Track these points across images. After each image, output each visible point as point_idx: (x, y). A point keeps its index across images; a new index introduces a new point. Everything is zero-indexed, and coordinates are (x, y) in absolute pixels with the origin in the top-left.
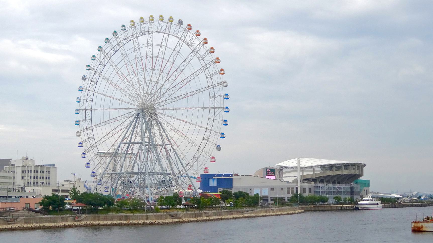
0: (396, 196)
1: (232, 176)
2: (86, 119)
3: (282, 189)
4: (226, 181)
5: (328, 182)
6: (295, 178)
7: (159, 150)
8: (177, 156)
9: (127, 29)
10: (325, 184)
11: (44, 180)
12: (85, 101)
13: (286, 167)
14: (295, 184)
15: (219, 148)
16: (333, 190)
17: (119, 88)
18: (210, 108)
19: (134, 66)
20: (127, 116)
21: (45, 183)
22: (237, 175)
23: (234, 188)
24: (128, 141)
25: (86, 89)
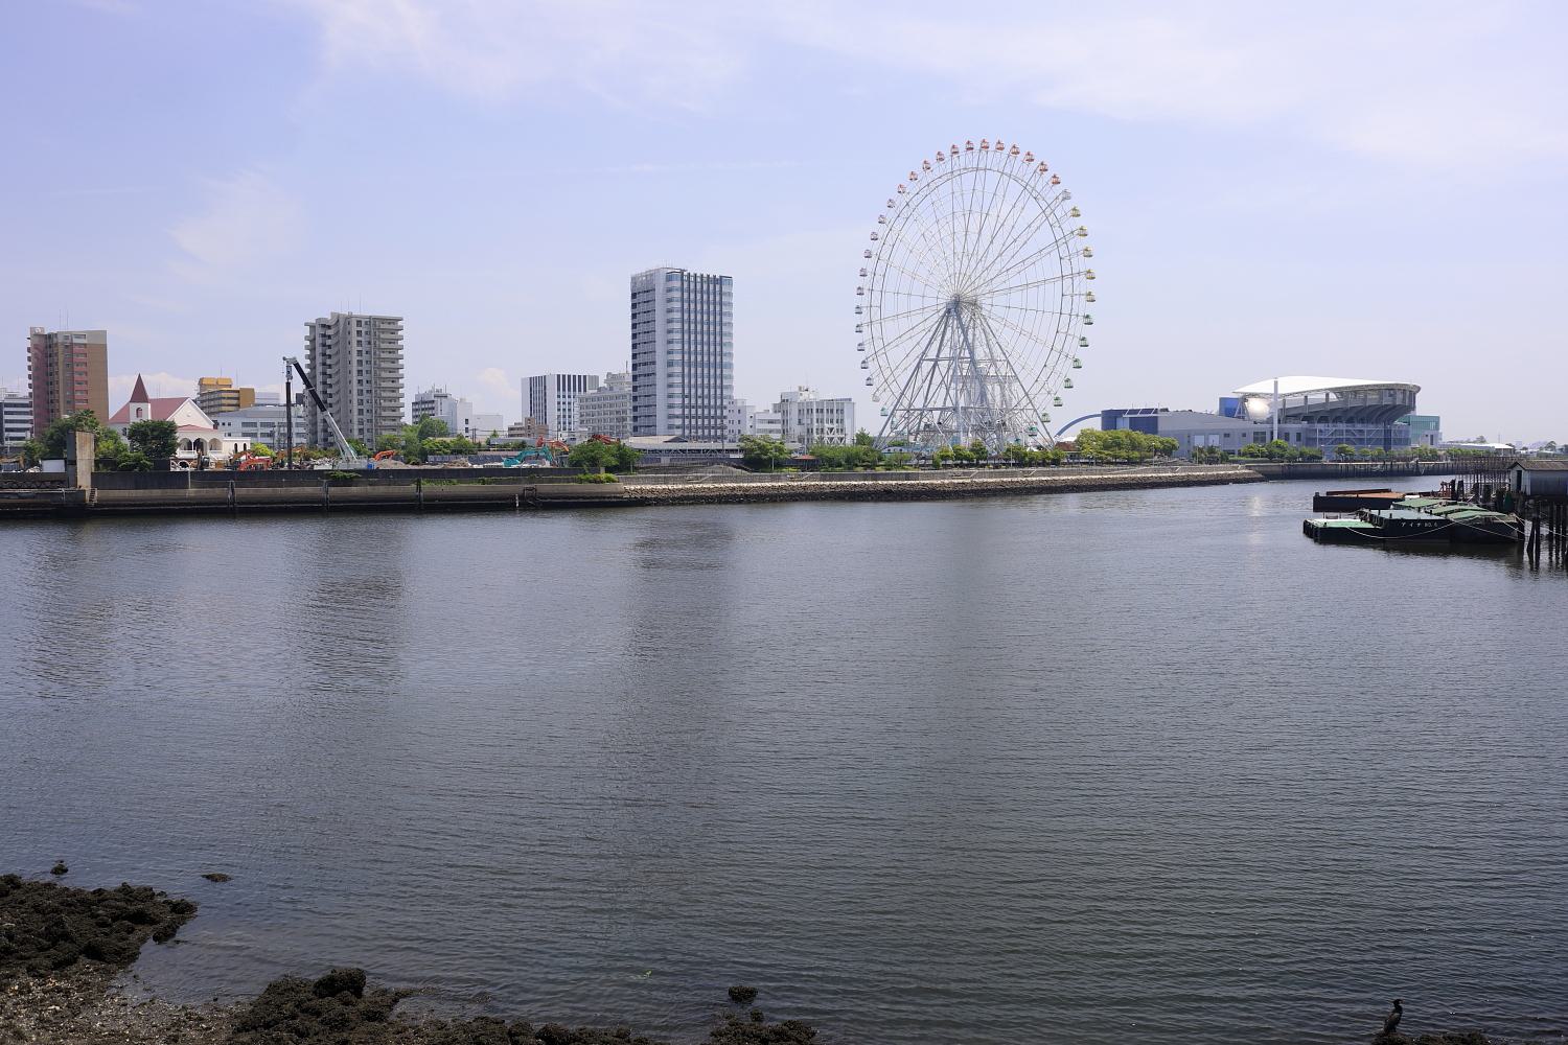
1: (1156, 411)
3: (1244, 435)
4: (1146, 421)
5: (1337, 420)
8: (932, 378)
11: (835, 426)
13: (1254, 395)
14: (1268, 426)
22: (1167, 410)
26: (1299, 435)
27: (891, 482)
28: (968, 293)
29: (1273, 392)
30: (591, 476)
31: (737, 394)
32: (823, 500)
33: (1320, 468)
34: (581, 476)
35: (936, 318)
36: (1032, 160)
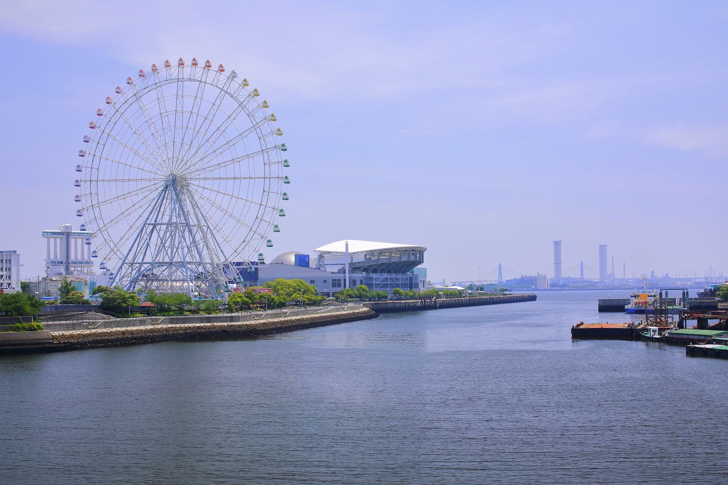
0: (460, 288)
3: (325, 281)
5: (383, 271)
6: (343, 266)
7: (194, 232)
8: (217, 242)
10: (379, 274)
14: (342, 275)
16: (389, 282)
18: (265, 178)
21: (4, 276)
23: (259, 280)
24: (153, 222)
26: (361, 281)
27: (223, 324)
28: (178, 172)
29: (344, 250)
30: (26, 325)
31: (662, 276)
32: (159, 341)
33: (385, 305)
34: (18, 324)
35: (157, 193)
36: (223, 71)
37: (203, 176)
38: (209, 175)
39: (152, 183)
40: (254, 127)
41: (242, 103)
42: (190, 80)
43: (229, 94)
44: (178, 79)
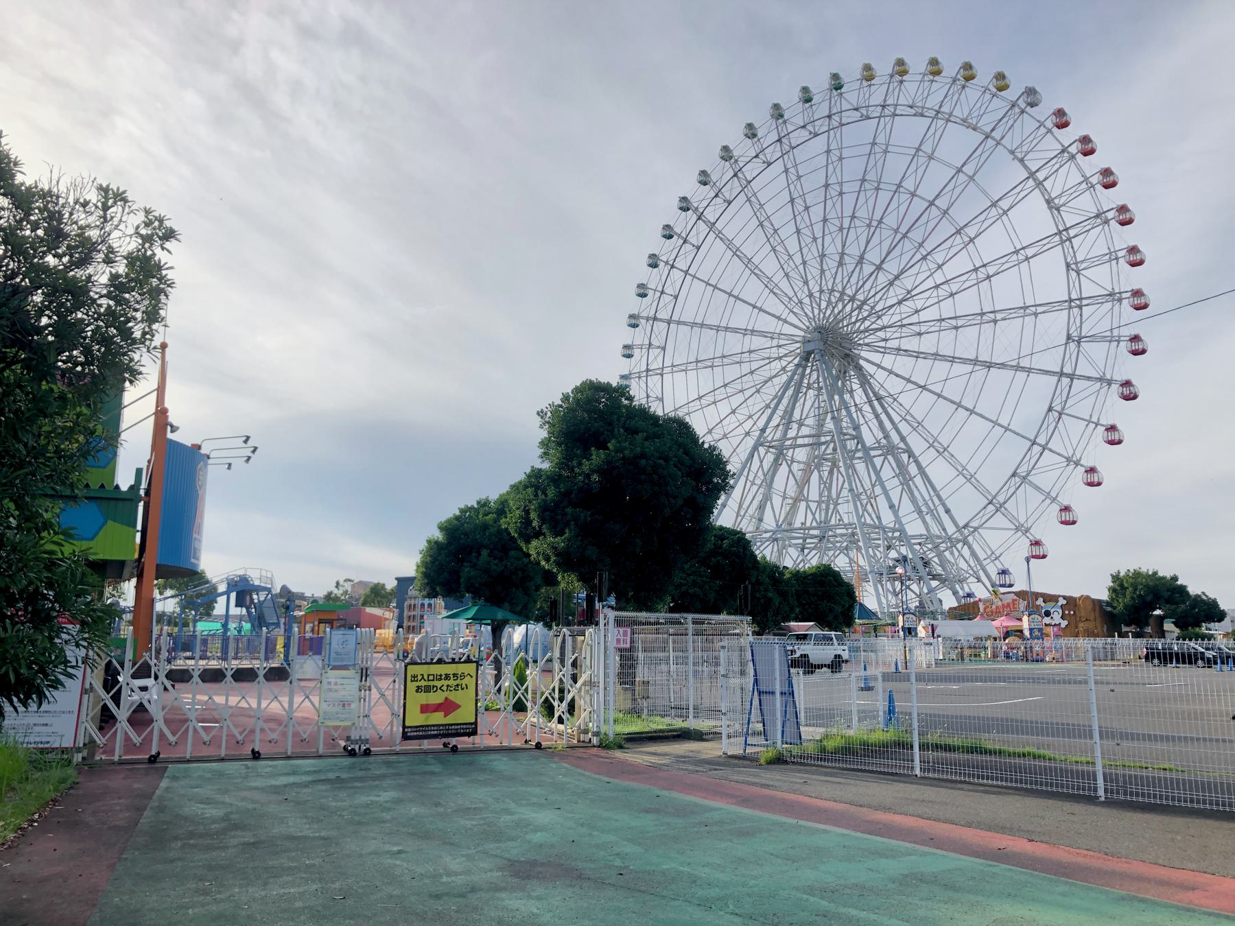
2: (650, 344)
9: (759, 135)
12: (658, 294)
15: (1093, 479)
17: (756, 271)
19: (849, 200)
20: (766, 354)
25: (667, 263)
37: (893, 344)
38: (911, 344)
39: (775, 342)
40: (1074, 303)
41: (1066, 229)
42: (964, 122)
43: (1044, 191)
44: (938, 112)
